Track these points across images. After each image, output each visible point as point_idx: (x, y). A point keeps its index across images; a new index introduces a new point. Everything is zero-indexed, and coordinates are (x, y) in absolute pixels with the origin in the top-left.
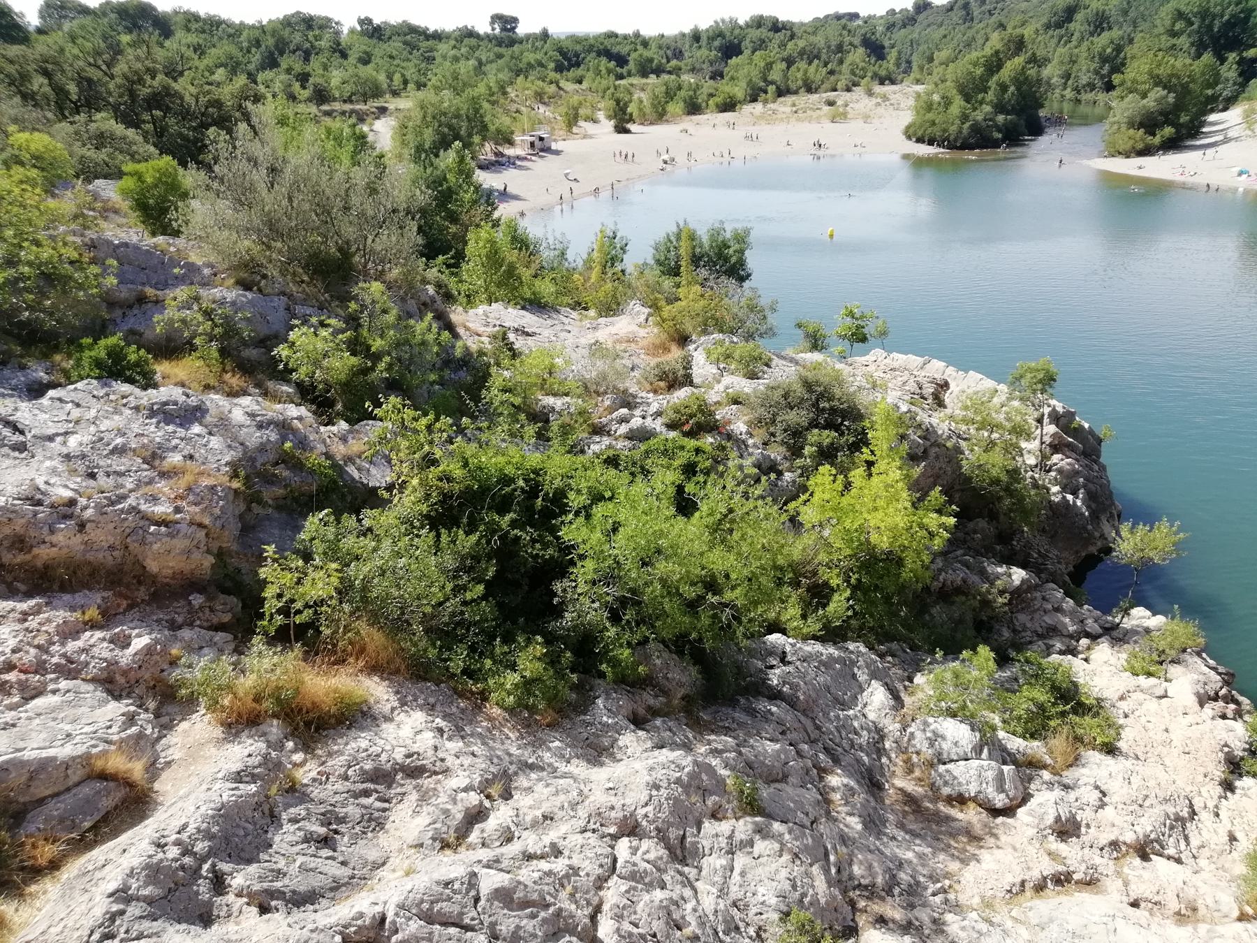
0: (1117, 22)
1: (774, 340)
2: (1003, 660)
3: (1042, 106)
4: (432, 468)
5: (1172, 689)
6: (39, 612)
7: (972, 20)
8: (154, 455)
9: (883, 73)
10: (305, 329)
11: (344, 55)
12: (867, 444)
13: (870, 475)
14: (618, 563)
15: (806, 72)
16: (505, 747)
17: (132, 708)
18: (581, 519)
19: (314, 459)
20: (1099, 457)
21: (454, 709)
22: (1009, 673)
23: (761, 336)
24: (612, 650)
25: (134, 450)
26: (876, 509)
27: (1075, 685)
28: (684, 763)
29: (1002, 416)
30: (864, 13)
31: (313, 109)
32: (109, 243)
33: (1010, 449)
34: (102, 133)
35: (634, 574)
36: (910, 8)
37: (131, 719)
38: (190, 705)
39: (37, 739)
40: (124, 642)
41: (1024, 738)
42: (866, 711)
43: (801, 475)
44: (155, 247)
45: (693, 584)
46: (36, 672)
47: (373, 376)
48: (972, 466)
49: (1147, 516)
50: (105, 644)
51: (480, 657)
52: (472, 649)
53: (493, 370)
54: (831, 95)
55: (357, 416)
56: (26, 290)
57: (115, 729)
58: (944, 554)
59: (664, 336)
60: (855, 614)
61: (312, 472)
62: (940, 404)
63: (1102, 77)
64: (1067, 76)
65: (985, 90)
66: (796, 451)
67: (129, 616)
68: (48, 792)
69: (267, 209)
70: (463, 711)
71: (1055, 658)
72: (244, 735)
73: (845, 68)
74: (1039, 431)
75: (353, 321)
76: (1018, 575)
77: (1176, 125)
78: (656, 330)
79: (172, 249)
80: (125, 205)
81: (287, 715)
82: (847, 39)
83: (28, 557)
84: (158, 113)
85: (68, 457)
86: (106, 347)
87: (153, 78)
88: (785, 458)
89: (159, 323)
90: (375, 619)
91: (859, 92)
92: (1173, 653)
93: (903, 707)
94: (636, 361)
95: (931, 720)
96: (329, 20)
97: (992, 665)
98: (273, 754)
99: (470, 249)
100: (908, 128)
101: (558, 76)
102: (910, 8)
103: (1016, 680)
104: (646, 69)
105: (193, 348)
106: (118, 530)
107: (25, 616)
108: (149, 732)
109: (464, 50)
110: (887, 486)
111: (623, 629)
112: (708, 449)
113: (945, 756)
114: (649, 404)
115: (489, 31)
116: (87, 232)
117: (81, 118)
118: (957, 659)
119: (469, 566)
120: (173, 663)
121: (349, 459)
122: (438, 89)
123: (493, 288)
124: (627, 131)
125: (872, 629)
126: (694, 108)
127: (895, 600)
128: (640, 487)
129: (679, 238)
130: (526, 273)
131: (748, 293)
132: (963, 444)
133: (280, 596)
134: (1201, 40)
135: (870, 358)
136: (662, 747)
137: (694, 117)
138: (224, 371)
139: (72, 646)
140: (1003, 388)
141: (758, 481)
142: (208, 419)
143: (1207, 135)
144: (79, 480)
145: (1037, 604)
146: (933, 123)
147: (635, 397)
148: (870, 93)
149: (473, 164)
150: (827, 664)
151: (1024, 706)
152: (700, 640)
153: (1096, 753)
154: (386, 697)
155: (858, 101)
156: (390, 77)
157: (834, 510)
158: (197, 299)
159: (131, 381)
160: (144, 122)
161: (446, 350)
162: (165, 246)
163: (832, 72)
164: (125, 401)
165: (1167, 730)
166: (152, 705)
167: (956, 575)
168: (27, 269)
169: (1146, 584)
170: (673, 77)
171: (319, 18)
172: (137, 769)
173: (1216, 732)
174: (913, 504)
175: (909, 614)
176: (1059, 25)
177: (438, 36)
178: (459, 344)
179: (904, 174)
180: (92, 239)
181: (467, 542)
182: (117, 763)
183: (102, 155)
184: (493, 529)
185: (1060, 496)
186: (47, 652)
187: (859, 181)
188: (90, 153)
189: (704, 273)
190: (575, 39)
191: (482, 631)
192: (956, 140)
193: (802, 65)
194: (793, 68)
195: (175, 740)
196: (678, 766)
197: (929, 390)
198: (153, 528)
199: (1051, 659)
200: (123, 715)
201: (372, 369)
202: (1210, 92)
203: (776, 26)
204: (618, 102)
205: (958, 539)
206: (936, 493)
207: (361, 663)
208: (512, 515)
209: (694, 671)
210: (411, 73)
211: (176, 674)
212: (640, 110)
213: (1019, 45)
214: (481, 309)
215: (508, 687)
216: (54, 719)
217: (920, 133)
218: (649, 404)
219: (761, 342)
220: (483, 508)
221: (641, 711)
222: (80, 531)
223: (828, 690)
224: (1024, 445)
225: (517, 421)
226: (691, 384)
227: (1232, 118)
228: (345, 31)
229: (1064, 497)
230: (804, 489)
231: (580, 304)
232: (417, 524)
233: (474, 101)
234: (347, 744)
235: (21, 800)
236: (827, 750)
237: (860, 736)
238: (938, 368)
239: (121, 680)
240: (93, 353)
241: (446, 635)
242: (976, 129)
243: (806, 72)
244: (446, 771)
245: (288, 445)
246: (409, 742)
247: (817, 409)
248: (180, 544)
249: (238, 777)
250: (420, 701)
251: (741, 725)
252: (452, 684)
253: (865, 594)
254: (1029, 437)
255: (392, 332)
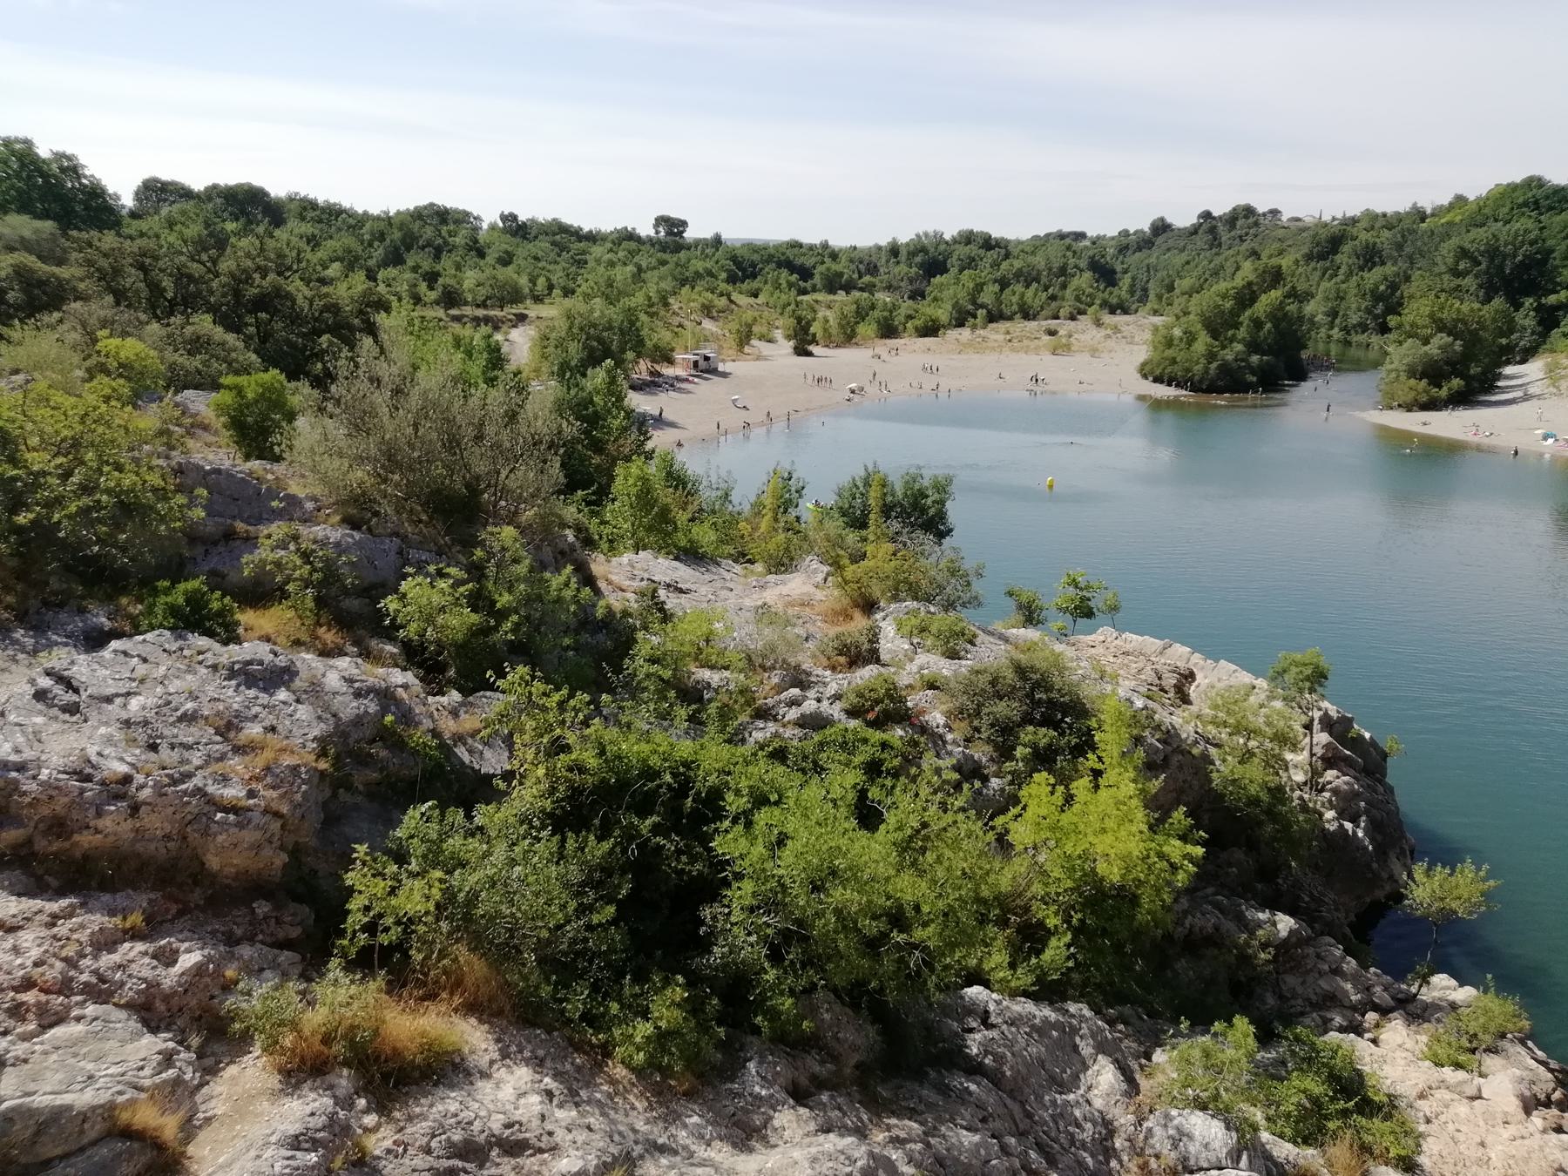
0: (1391, 257)
1: (980, 611)
2: (1266, 1037)
3: (1305, 347)
4: (562, 756)
5: (1488, 1087)
6: (71, 916)
7: (1220, 245)
8: (229, 726)
9: (1114, 301)
10: (419, 579)
11: (481, 254)
12: (1094, 748)
13: (1097, 787)
14: (783, 886)
16: (630, 1120)
17: (171, 1045)
18: (740, 828)
19: (419, 737)
20: (1384, 775)
21: (568, 1066)
22: (1274, 1054)
23: (964, 605)
24: (771, 998)
25: (206, 718)
26: (1104, 831)
27: (1360, 1074)
28: (856, 1155)
29: (1261, 720)
30: (1092, 233)
31: (440, 312)
32: (199, 468)
33: (1272, 762)
34: (198, 338)
35: (800, 898)
36: (1146, 229)
37: (168, 1059)
38: (241, 1043)
39: (53, 1080)
40: (167, 958)
41: (1295, 1143)
42: (1091, 1095)
43: (1011, 783)
44: (251, 474)
45: (875, 917)
46: (59, 993)
47: (496, 637)
48: (1225, 780)
49: (1446, 855)
50: (147, 960)
51: (604, 999)
52: (595, 988)
53: (640, 635)
54: (1053, 323)
55: (473, 684)
56: (99, 521)
57: (147, 1072)
58: (1190, 891)
59: (846, 601)
60: (1078, 964)
61: (414, 752)
62: (1185, 700)
63: (1376, 317)
64: (1333, 314)
65: (1237, 326)
66: (1005, 752)
67: (179, 925)
68: (58, 1151)
69: (387, 437)
70: (579, 1069)
71: (1333, 1036)
72: (306, 1086)
73: (1068, 292)
74: (1307, 740)
75: (476, 571)
76: (1285, 924)
77: (1466, 376)
78: (836, 593)
79: (270, 477)
80: (218, 422)
81: (360, 1063)
83: (67, 845)
84: (263, 315)
85: (127, 723)
86: (186, 592)
87: (264, 277)
88: (992, 759)
89: (249, 562)
90: (477, 942)
91: (1085, 321)
92: (1487, 1039)
93: (1138, 1094)
94: (812, 629)
95: (1174, 1112)
96: (467, 214)
97: (1251, 1042)
98: (342, 1114)
99: (618, 486)
100: (1144, 365)
101: (730, 288)
102: (1146, 229)
103: (1284, 1063)
104: (834, 284)
105: (285, 595)
106: (178, 816)
107: (54, 919)
108: (188, 1077)
109: (621, 254)
110: (1118, 803)
111: (786, 972)
112: (897, 743)
113: (1192, 1162)
114: (825, 684)
115: (652, 233)
116: (174, 453)
117: (177, 320)
118: (1208, 1032)
119: (598, 880)
120: (228, 987)
121: (459, 738)
122: (587, 297)
123: (641, 534)
124: (809, 354)
125: (1098, 986)
126: (889, 331)
127: (1128, 949)
128: (814, 791)
129: (867, 484)
130: (682, 517)
131: (949, 554)
132: (1213, 751)
133: (367, 909)
134: (1490, 281)
135: (1097, 637)
136: (828, 1131)
137: (888, 341)
138: (318, 624)
139: (107, 960)
140: (1262, 683)
141: (958, 787)
142: (297, 683)
143: (1503, 390)
144: (138, 751)
145: (1310, 963)
147: (808, 674)
148: (1098, 323)
149: (625, 385)
150: (1042, 1030)
151: (1294, 1100)
152: (881, 990)
153: (1390, 1170)
154: (484, 1046)
155: (1084, 331)
156: (533, 281)
157: (1053, 829)
158: (296, 538)
159: (210, 634)
160: (246, 324)
161: (586, 610)
162: (261, 473)
163: (1053, 298)
164: (201, 657)
165: (1482, 1144)
166: (195, 1041)
167: (1206, 920)
168: (105, 497)
169: (1453, 944)
170: (866, 295)
171: (457, 211)
172: (168, 1126)
173: (1547, 1150)
174: (1151, 828)
175: (1146, 969)
176: (1322, 257)
177: (592, 238)
178: (602, 603)
179: (1140, 417)
180: (180, 464)
181: (598, 849)
182: (147, 1116)
183: (196, 362)
184: (630, 834)
185: (1336, 824)
186: (75, 966)
187: (1084, 421)
188: (181, 359)
189: (896, 525)
190: (753, 247)
191: (609, 965)
192: (1201, 381)
193: (1019, 288)
194: (1007, 291)
195: (219, 1089)
196: (848, 1158)
197: (1170, 681)
198: (219, 815)
199: (1327, 1038)
200: (159, 1053)
201: (496, 629)
202: (1504, 341)
203: (988, 243)
204: (799, 320)
205: (1207, 873)
206: (1179, 815)
207: (457, 1000)
208: (655, 818)
209: (872, 1031)
210: (558, 277)
211: (230, 1002)
212: (825, 330)
213: (1275, 277)
214: (626, 558)
215: (638, 1039)
216: (75, 1055)
217: (1158, 372)
218: (825, 684)
219: (964, 613)
220: (619, 808)
221: (804, 1081)
222: (132, 816)
223: (1042, 1064)
224: (1289, 756)
225: (665, 699)
226: (878, 661)
227: (1533, 370)
228: (485, 226)
229: (1341, 826)
230: (1014, 800)
231: (744, 555)
232: (536, 823)
233: (630, 313)
234: (431, 1106)
235: (23, 1160)
236: (1040, 1147)
237: (1083, 1130)
238: (1180, 655)
239: (160, 1007)
240: (169, 599)
241: (562, 966)
242: (1225, 369)
243: (1023, 295)
244: (554, 1149)
245: (389, 718)
246: (509, 1107)
247: (1032, 700)
248: (249, 836)
249: (295, 1143)
250: (527, 1054)
251: (931, 1107)
252: (567, 1032)
253: (1089, 940)
254: (1295, 747)
255: (522, 587)
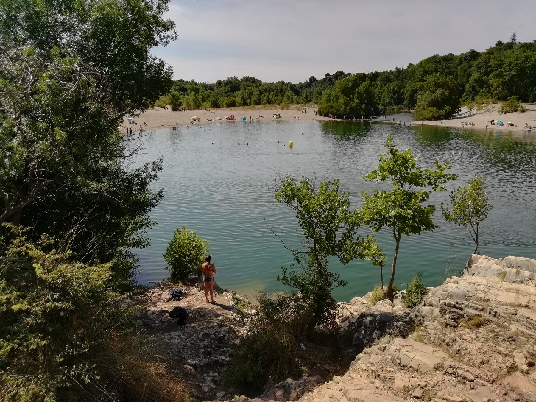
15: (268, 97)
77: (448, 106)
82: (284, 87)
146: (332, 107)
194: (262, 95)
243: (268, 97)
